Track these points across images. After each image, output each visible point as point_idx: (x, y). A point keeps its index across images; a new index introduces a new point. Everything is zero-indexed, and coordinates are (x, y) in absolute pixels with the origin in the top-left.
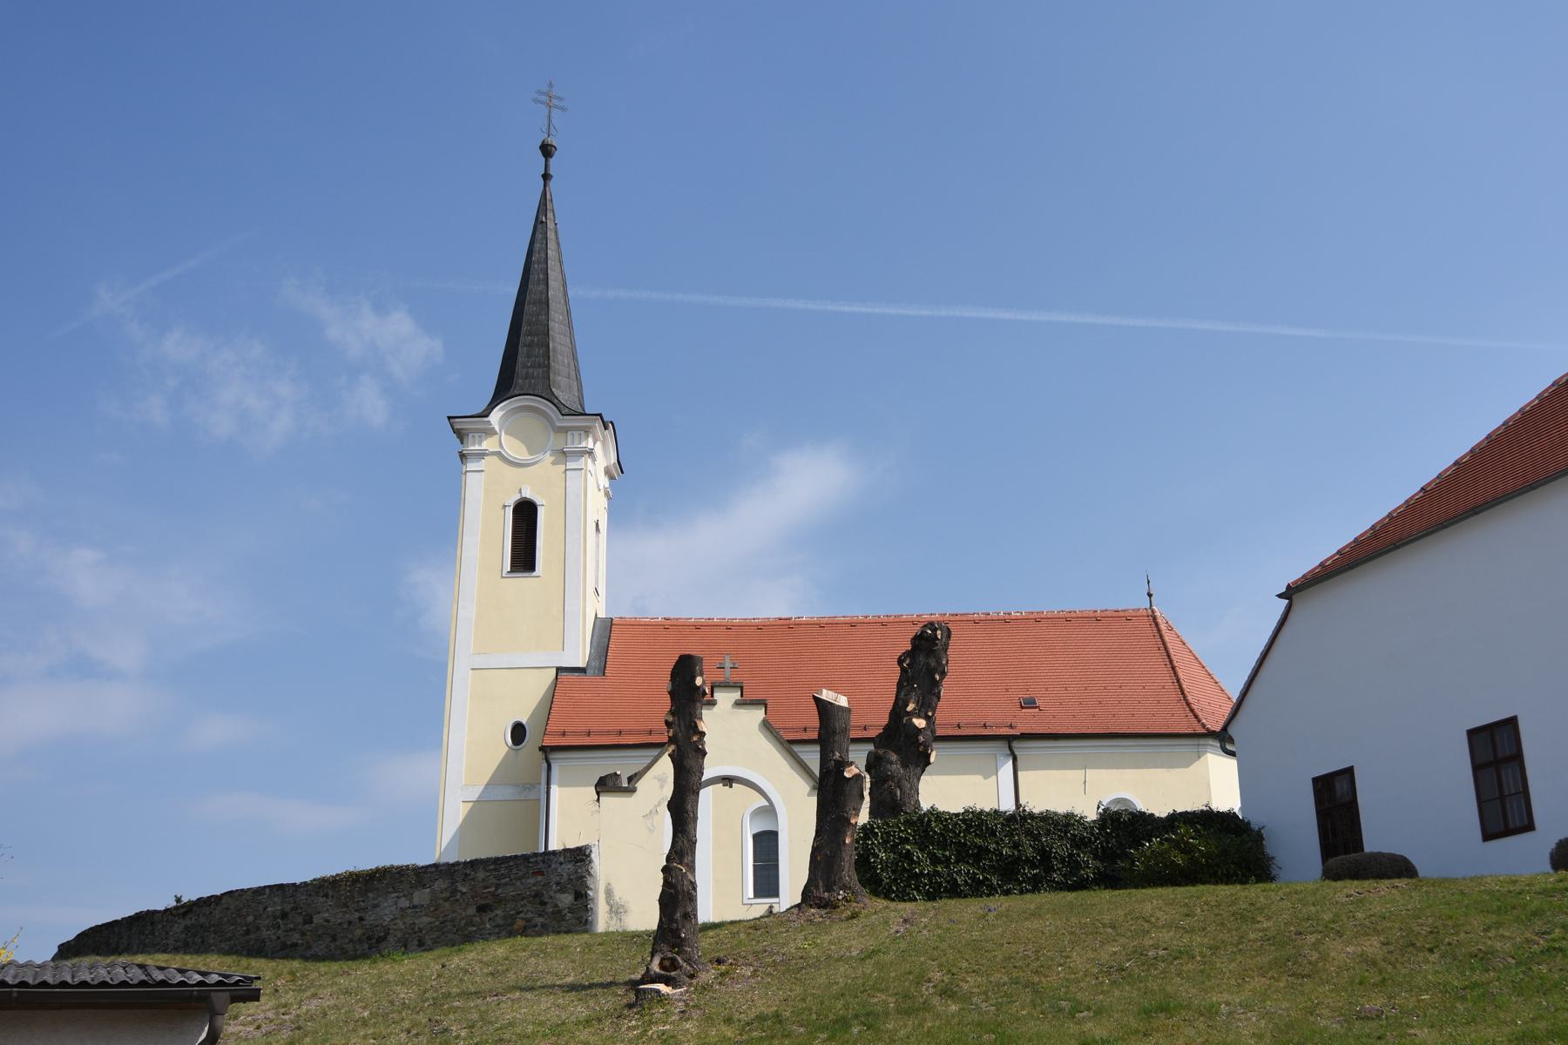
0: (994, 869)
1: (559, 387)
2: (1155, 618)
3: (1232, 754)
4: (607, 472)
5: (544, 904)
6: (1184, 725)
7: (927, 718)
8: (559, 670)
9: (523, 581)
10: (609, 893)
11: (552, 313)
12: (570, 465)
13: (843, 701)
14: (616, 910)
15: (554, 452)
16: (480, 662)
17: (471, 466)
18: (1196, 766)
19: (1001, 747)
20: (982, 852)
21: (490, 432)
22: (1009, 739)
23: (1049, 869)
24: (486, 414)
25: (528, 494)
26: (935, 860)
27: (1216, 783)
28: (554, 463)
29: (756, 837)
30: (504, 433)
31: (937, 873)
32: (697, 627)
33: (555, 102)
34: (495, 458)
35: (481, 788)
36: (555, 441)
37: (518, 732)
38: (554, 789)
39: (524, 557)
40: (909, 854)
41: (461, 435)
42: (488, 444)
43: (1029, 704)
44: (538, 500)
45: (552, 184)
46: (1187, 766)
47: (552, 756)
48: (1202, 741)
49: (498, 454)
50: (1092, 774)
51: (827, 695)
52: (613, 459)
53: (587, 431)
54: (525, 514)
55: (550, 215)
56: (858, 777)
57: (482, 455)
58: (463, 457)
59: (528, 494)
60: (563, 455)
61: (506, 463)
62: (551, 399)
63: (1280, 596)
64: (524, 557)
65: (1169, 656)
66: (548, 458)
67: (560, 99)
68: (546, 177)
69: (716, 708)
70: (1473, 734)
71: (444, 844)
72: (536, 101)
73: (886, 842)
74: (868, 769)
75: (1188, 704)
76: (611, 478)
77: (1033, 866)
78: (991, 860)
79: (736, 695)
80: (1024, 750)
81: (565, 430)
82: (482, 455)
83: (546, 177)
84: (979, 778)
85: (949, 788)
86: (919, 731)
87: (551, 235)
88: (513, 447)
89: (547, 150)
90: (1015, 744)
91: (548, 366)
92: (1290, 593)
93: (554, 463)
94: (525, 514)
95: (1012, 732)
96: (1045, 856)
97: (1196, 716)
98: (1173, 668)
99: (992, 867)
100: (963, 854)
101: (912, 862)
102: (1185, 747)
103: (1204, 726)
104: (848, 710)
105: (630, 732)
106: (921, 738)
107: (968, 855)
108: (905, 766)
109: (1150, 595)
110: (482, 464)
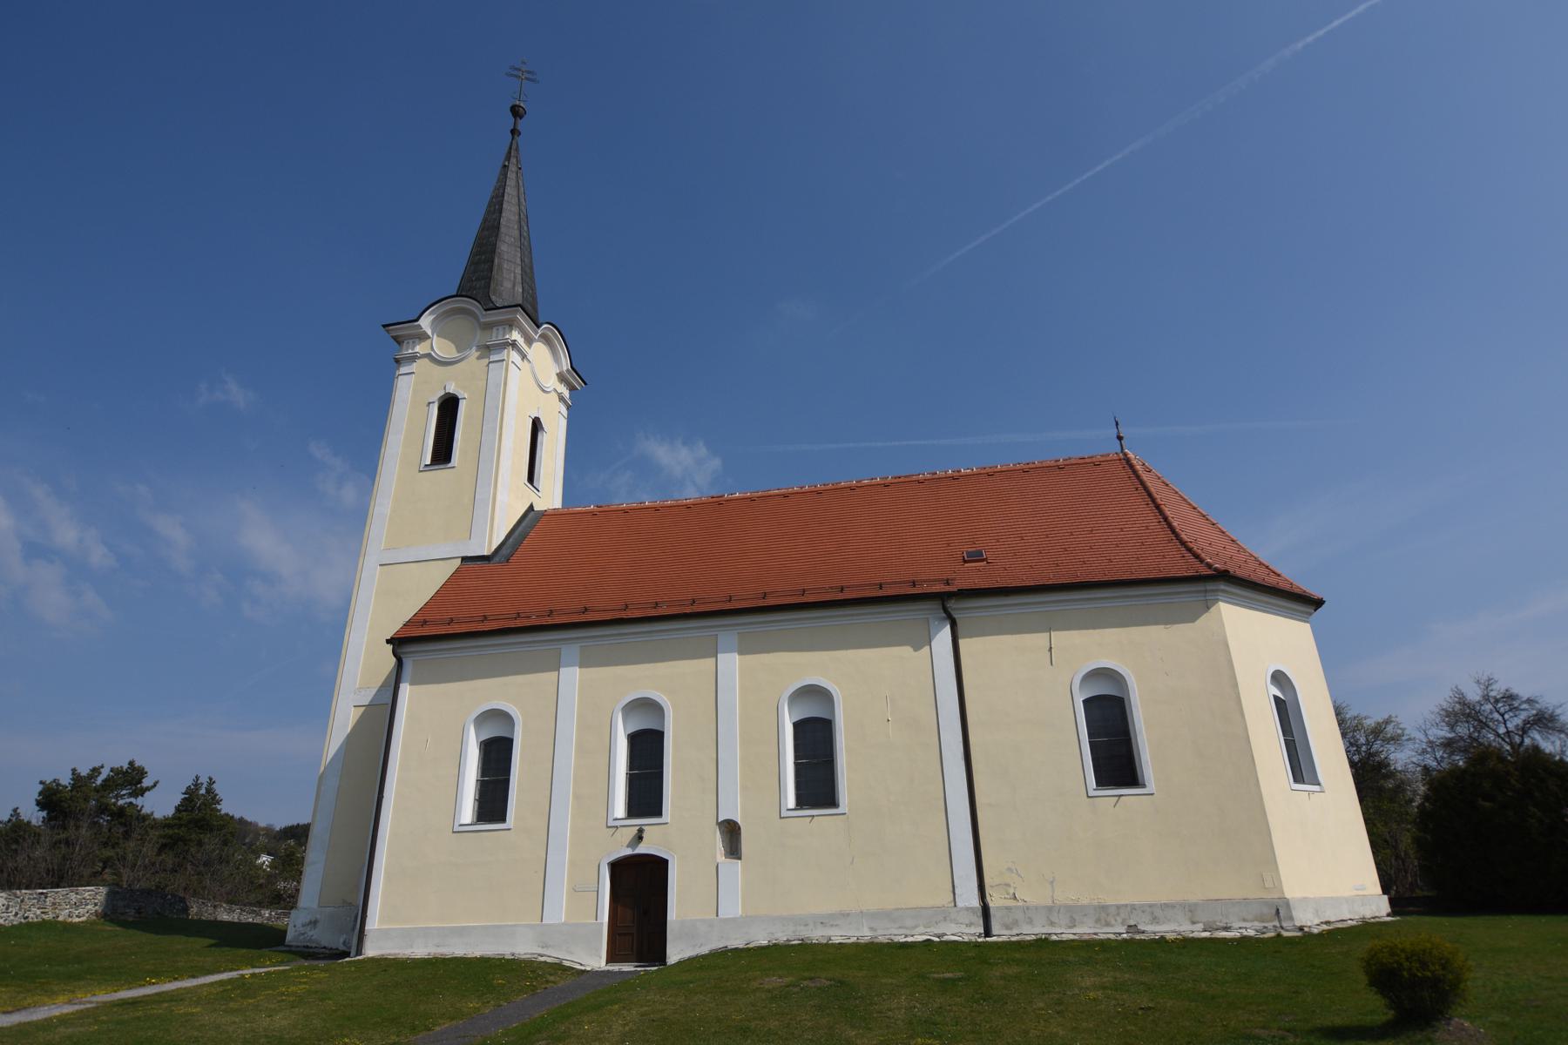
2: (1128, 461)
4: (562, 378)
6: (1180, 565)
8: (464, 559)
9: (441, 474)
12: (493, 358)
15: (479, 348)
17: (403, 370)
18: (1203, 620)
19: (930, 610)
21: (423, 337)
22: (942, 598)
29: (799, 727)
32: (625, 511)
35: (374, 691)
36: (480, 337)
38: (406, 689)
39: (442, 452)
42: (420, 348)
43: (976, 557)
46: (1193, 619)
48: (1210, 586)
49: (428, 356)
50: (1061, 638)
52: (566, 365)
53: (511, 324)
54: (449, 406)
55: (513, 160)
57: (413, 358)
58: (397, 361)
64: (442, 452)
65: (1150, 495)
66: (474, 353)
70: (666, 862)
71: (330, 756)
75: (1183, 543)
80: (965, 611)
81: (488, 327)
83: (514, 132)
84: (906, 651)
88: (441, 346)
89: (516, 112)
90: (952, 604)
94: (449, 406)
95: (947, 589)
97: (1197, 556)
98: (1158, 507)
102: (1184, 597)
103: (1209, 566)
109: (1120, 438)
110: (414, 367)
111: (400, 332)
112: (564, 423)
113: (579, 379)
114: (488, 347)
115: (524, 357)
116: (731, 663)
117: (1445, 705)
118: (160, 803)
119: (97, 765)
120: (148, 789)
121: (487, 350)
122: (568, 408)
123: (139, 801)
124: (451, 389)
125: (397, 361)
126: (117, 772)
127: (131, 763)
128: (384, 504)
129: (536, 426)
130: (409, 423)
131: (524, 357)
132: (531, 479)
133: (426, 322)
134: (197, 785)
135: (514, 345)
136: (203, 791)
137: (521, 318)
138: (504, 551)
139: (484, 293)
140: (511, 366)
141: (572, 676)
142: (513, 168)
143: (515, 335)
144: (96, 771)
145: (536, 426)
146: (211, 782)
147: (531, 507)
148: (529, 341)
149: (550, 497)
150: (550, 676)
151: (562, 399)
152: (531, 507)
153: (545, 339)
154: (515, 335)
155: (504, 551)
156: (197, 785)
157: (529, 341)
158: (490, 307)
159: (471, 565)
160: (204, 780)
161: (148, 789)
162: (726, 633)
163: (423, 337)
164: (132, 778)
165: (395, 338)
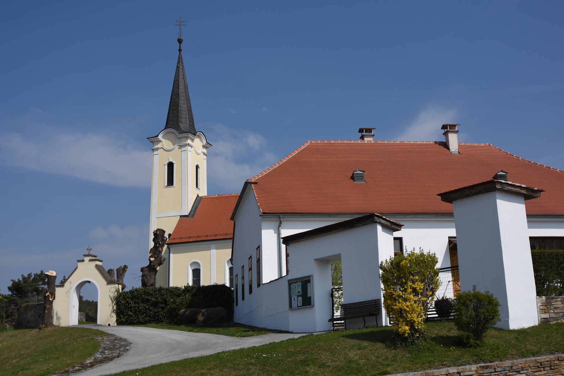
1: (182, 123)
4: (204, 147)
7: (155, 258)
8: (181, 216)
9: (170, 189)
10: (57, 314)
12: (183, 149)
14: (58, 318)
16: (159, 216)
17: (155, 153)
20: (148, 300)
24: (157, 136)
30: (165, 143)
38: (171, 255)
39: (170, 182)
40: (128, 301)
42: (159, 146)
45: (182, 52)
52: (205, 142)
53: (187, 138)
54: (171, 166)
55: (181, 63)
56: (48, 295)
57: (157, 149)
61: (166, 149)
64: (170, 182)
66: (177, 147)
67: (184, 22)
68: (180, 50)
73: (123, 298)
81: (180, 138)
82: (157, 149)
83: (180, 50)
89: (180, 41)
91: (178, 116)
92: (232, 218)
94: (171, 166)
100: (143, 301)
104: (55, 277)
108: (149, 272)
111: (154, 140)
112: (205, 161)
115: (191, 146)
117: (112, 295)
121: (181, 147)
124: (171, 160)
126: (36, 275)
127: (42, 272)
131: (191, 146)
132: (197, 186)
133: (160, 137)
135: (189, 145)
138: (192, 213)
141: (214, 252)
142: (181, 67)
143: (189, 141)
144: (30, 275)
147: (198, 196)
148: (193, 140)
149: (203, 192)
150: (209, 251)
151: (204, 154)
152: (198, 196)
153: (199, 137)
154: (189, 141)
155: (192, 213)
157: (193, 140)
159: (183, 218)
163: (160, 141)
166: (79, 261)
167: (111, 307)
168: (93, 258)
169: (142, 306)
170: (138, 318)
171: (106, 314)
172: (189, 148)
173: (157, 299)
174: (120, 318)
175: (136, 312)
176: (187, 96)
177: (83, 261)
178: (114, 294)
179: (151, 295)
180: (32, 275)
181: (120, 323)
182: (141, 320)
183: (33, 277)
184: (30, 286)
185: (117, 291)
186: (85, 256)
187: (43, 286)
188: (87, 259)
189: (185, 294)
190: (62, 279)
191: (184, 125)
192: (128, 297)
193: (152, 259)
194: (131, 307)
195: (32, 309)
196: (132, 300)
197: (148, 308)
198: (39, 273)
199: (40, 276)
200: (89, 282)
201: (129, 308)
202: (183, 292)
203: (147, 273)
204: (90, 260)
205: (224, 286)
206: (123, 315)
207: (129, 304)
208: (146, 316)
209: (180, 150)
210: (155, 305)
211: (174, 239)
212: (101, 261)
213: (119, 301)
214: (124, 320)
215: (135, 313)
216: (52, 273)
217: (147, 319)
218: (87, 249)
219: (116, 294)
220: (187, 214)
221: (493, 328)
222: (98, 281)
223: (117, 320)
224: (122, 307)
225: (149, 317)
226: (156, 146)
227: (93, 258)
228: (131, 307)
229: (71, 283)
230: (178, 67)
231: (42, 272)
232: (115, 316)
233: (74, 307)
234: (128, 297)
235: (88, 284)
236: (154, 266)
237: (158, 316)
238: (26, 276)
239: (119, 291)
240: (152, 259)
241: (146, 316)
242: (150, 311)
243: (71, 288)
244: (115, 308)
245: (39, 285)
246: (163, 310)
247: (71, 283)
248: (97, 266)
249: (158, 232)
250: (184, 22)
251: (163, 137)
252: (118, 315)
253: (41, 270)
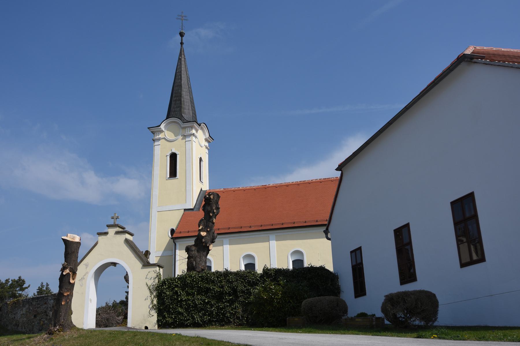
0: (213, 297)
3: (329, 239)
4: (206, 140)
5: (47, 315)
7: (207, 231)
8: (185, 210)
9: (173, 181)
11: (183, 89)
12: (187, 139)
13: (77, 239)
17: (156, 143)
20: (208, 290)
21: (162, 131)
23: (237, 297)
24: (160, 126)
25: (174, 151)
26: (188, 294)
27: (318, 252)
28: (182, 139)
29: (293, 261)
31: (189, 300)
32: (234, 191)
33: (184, 18)
34: (163, 140)
37: (172, 231)
39: (173, 173)
40: (176, 292)
41: (153, 133)
42: (161, 136)
44: (177, 153)
45: (184, 46)
47: (176, 240)
49: (164, 138)
51: (63, 237)
52: (207, 135)
53: (192, 127)
54: (173, 157)
55: (183, 56)
56: (68, 274)
57: (159, 139)
59: (174, 151)
60: (185, 137)
62: (181, 118)
63: (337, 170)
64: (173, 173)
66: (180, 137)
67: (185, 16)
69: (108, 236)
72: (177, 19)
73: (169, 287)
74: (70, 271)
76: (209, 142)
77: (230, 296)
78: (212, 293)
79: (118, 229)
81: (184, 128)
83: (182, 43)
85: (226, 257)
86: (203, 237)
87: (183, 63)
88: (168, 134)
89: (182, 35)
91: (181, 107)
93: (182, 139)
94: (173, 157)
96: (234, 291)
99: (213, 296)
101: (178, 296)
104: (79, 244)
105: (192, 232)
106: (203, 240)
107: (202, 292)
108: (198, 251)
111: (154, 130)
112: (207, 155)
113: (210, 139)
114: (185, 136)
115: (196, 137)
116: (274, 244)
117: (150, 283)
118: (31, 292)
119: (7, 278)
120: (27, 288)
121: (185, 137)
122: (208, 149)
123: (24, 293)
125: (154, 140)
126: (14, 281)
127: (20, 278)
128: (156, 193)
129: (201, 160)
130: (161, 165)
131: (196, 137)
133: (162, 127)
134: (42, 286)
135: (193, 135)
136: (45, 289)
137: (195, 125)
138: (197, 207)
139: (178, 111)
140: (193, 142)
142: (183, 59)
143: (194, 131)
144: (7, 281)
145: (201, 160)
146: (47, 285)
148: (197, 131)
149: (206, 187)
151: (207, 148)
153: (202, 129)
154: (194, 131)
156: (42, 286)
157: (197, 131)
158: (185, 121)
160: (45, 284)
161: (27, 288)
162: (272, 235)
163: (162, 131)
164: (20, 283)
165: (152, 132)
166: (100, 234)
167: (149, 301)
168: (121, 230)
169: (199, 299)
170: (193, 318)
171: (142, 314)
172: (194, 138)
173: (222, 287)
174: (164, 317)
175: (189, 307)
176: (190, 88)
177: (106, 233)
178: (153, 282)
179: (213, 282)
180: (10, 280)
181: (160, 327)
182: (197, 319)
183: (11, 282)
184: (8, 292)
185: (158, 276)
186: (109, 226)
187: (20, 292)
188: (112, 231)
189: (265, 281)
190: (40, 285)
191: (187, 114)
192: (177, 286)
193: (203, 234)
194: (181, 300)
195: (24, 306)
196: (183, 290)
197: (208, 302)
198: (17, 278)
199: (17, 282)
200: (114, 264)
201: (179, 301)
202: (260, 277)
203: (195, 253)
204: (117, 233)
205: (322, 269)
206: (169, 312)
207: (178, 296)
208: (204, 315)
209: (184, 141)
210: (219, 297)
211: (180, 232)
212: (132, 235)
213: (162, 291)
214: (170, 320)
215: (186, 310)
216: (73, 238)
217: (206, 318)
218: (113, 218)
219: (157, 281)
220: (192, 207)
221: (435, 327)
222: (129, 263)
223: (158, 321)
224: (167, 301)
225: (209, 315)
226: (158, 137)
227: (121, 230)
228: (181, 300)
229: (87, 265)
230: (180, 59)
231: (20, 278)
232: (156, 315)
233: (91, 301)
234: (177, 286)
235: (112, 267)
236: (206, 244)
237: (224, 314)
238: (4, 282)
239: (160, 278)
240: (203, 234)
241: (204, 315)
242: (212, 306)
243: (87, 273)
244: (155, 302)
245: (16, 290)
246: (230, 306)
247: (87, 265)
248: (127, 241)
249: (212, 197)
250: (185, 16)
251: (165, 127)
252: (160, 313)
253: (19, 276)
